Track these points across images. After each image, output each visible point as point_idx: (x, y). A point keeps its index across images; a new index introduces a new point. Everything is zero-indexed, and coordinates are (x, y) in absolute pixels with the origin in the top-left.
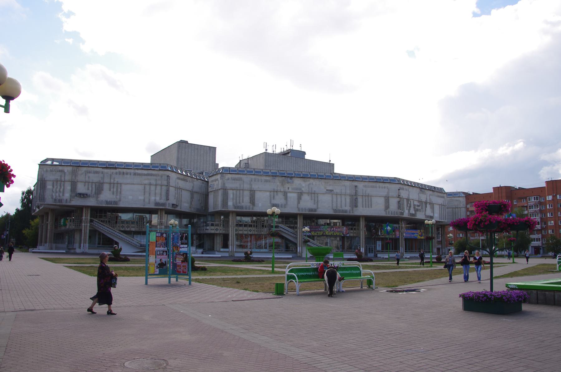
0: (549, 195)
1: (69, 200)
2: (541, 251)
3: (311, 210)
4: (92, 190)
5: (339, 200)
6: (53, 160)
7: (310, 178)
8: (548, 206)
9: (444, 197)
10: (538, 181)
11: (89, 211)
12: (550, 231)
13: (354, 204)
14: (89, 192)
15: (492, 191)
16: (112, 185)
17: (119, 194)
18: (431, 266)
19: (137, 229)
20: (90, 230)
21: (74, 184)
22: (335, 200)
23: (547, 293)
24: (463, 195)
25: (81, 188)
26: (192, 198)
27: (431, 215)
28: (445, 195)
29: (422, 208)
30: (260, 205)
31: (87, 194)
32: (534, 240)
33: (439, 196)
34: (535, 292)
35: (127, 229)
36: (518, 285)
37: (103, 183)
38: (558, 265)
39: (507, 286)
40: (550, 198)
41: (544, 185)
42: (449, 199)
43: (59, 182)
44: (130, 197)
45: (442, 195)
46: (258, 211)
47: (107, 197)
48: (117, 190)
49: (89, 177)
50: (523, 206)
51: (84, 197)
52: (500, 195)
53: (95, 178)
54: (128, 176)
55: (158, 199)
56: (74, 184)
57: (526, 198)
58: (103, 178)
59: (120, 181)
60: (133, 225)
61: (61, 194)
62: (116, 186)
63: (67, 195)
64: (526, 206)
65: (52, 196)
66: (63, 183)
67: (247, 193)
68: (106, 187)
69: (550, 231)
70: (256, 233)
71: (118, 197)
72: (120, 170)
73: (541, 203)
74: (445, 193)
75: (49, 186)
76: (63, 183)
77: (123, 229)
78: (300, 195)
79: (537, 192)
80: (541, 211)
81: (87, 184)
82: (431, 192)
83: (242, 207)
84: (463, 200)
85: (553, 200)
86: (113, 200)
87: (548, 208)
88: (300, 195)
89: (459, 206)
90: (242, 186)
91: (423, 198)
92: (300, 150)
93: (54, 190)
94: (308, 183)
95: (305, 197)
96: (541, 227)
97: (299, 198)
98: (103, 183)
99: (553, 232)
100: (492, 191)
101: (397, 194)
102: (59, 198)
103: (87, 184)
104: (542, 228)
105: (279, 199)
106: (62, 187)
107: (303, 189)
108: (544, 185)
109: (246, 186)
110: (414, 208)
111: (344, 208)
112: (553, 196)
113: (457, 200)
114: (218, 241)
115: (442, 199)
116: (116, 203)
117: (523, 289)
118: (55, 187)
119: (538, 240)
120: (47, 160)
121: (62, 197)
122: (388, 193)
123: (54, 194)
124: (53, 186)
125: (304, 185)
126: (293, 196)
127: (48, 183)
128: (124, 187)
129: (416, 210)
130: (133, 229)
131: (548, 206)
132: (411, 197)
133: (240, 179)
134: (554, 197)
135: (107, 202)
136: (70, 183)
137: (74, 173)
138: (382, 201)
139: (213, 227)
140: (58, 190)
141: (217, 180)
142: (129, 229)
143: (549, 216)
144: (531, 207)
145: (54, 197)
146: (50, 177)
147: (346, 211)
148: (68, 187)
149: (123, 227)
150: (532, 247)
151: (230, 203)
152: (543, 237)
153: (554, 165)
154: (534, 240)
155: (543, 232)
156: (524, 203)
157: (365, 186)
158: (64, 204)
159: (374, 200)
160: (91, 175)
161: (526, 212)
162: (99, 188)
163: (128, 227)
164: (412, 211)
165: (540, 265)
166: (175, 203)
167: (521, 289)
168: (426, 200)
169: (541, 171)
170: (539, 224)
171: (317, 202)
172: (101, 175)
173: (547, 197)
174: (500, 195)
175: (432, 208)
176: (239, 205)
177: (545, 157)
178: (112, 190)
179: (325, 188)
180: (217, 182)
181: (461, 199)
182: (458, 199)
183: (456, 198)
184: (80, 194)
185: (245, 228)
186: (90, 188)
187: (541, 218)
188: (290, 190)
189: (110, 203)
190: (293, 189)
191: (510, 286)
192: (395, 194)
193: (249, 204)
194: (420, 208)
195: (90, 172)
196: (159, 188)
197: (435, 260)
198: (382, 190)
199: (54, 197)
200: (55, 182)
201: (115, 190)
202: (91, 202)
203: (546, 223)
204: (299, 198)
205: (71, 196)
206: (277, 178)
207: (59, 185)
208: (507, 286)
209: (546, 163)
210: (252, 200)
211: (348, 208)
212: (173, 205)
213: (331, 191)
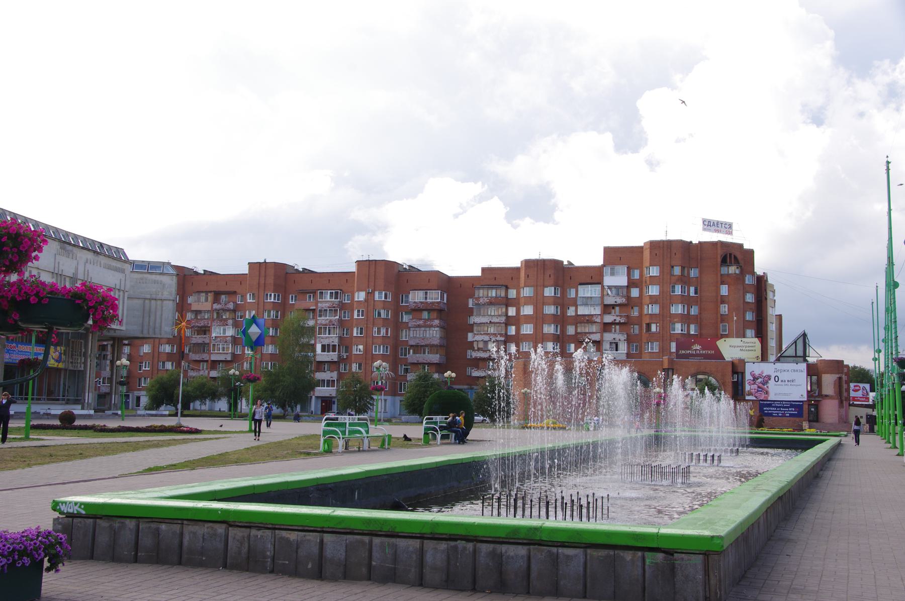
0: (359, 290)
2: (335, 407)
8: (356, 312)
9: (122, 271)
10: (345, 262)
12: (355, 367)
15: (245, 270)
18: (27, 438)
23: (163, 527)
24: (172, 271)
28: (128, 268)
32: (322, 383)
33: (109, 268)
38: (322, 439)
39: (56, 506)
40: (361, 296)
41: (353, 268)
42: (136, 276)
50: (308, 310)
52: (262, 282)
57: (314, 293)
64: (314, 310)
69: (355, 367)
73: (342, 306)
74: (127, 261)
79: (337, 282)
80: (341, 323)
82: (90, 256)
84: (171, 283)
85: (366, 300)
87: (355, 317)
89: (159, 296)
92: (664, 238)
96: (339, 356)
100: (245, 270)
104: (341, 360)
108: (353, 268)
112: (368, 294)
113: (155, 282)
115: (121, 276)
119: (330, 383)
131: (356, 312)
134: (370, 295)
143: (355, 334)
144: (323, 312)
150: (317, 397)
152: (341, 376)
154: (322, 383)
155: (342, 366)
156: (309, 303)
161: (311, 323)
165: (300, 438)
167: (95, 517)
168: (76, 273)
169: (350, 243)
170: (334, 351)
173: (356, 294)
174: (262, 282)
181: (165, 279)
182: (158, 278)
183: (153, 277)
187: (340, 338)
191: (64, 508)
197: (57, 422)
203: (348, 349)
208: (56, 506)
209: (360, 228)
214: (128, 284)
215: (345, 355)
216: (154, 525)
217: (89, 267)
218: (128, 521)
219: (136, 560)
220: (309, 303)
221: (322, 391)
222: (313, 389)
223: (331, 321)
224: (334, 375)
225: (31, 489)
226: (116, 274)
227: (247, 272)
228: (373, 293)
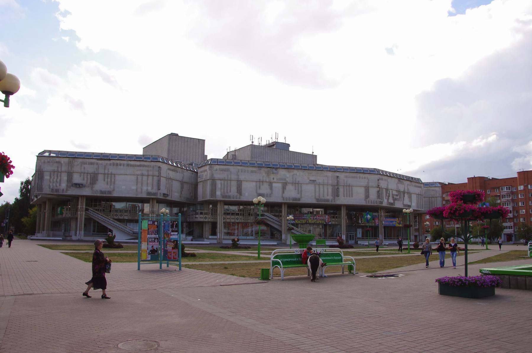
0: (520, 185)
1: (65, 190)
2: (513, 238)
3: (295, 199)
5: (321, 189)
7: (294, 169)
8: (520, 195)
9: (421, 187)
12: (521, 220)
13: (336, 193)
14: (84, 182)
15: (466, 181)
16: (106, 175)
17: (112, 184)
18: (409, 253)
19: (130, 218)
20: (85, 219)
21: (70, 175)
22: (317, 190)
23: (519, 278)
24: (439, 185)
25: (77, 179)
26: (182, 188)
27: (409, 204)
30: (247, 194)
31: (82, 185)
32: (506, 227)
33: (416, 186)
34: (507, 277)
35: (120, 218)
36: (491, 271)
38: (529, 252)
40: (521, 188)
41: (516, 176)
43: (56, 173)
44: (124, 187)
45: (417, 185)
47: (101, 187)
48: (111, 180)
49: (84, 168)
51: (80, 187)
53: (90, 169)
54: (122, 167)
55: (150, 188)
56: (70, 175)
57: (499, 188)
58: (368, 183)
59: (114, 171)
61: (58, 185)
62: (110, 177)
63: (64, 185)
64: (499, 196)
65: (49, 185)
66: (59, 174)
68: (100, 177)
69: (521, 220)
70: (243, 221)
72: (114, 161)
73: (513, 193)
75: (47, 177)
78: (285, 185)
79: (509, 182)
80: (513, 200)
82: (408, 183)
83: (229, 197)
84: (439, 190)
85: (524, 189)
87: (520, 197)
88: (285, 185)
89: (435, 196)
91: (401, 188)
93: (51, 180)
95: (290, 187)
96: (513, 215)
97: (284, 188)
99: (524, 220)
100: (466, 181)
101: (377, 184)
102: (56, 188)
103: (82, 174)
104: (514, 217)
105: (265, 189)
106: (59, 178)
107: (287, 179)
108: (516, 176)
109: (234, 177)
110: (393, 197)
111: (326, 197)
112: (525, 186)
113: (433, 190)
114: (207, 229)
116: (110, 192)
117: (496, 275)
118: (52, 177)
119: (510, 227)
120: (45, 152)
122: (368, 183)
123: (51, 184)
124: (50, 177)
125: (288, 176)
127: (45, 173)
128: (118, 178)
129: (395, 200)
130: (126, 218)
131: (520, 195)
132: (390, 187)
133: (228, 170)
134: (526, 187)
135: (101, 192)
136: (66, 174)
138: (362, 190)
139: (202, 216)
140: (55, 180)
141: (206, 170)
142: (122, 218)
144: (503, 196)
145: (52, 187)
146: (48, 168)
147: (328, 200)
148: (65, 178)
149: (116, 215)
150: (504, 234)
151: (218, 193)
152: (515, 225)
153: (525, 157)
154: (506, 227)
155: (515, 220)
156: (497, 192)
157: (346, 177)
159: (355, 189)
160: (86, 166)
161: (499, 201)
162: (94, 179)
164: (391, 201)
166: (166, 192)
167: (494, 275)
168: (404, 190)
169: (514, 162)
171: (300, 192)
172: (96, 166)
173: (519, 187)
176: (226, 194)
177: (517, 149)
178: (106, 180)
179: (308, 178)
181: (437, 189)
184: (76, 184)
186: (86, 179)
187: (513, 207)
188: (275, 180)
189: (105, 192)
190: (277, 179)
191: (483, 272)
192: (375, 184)
193: (236, 194)
194: (398, 197)
195: (85, 163)
196: (150, 178)
197: (413, 247)
198: (362, 181)
199: (52, 187)
201: (109, 180)
202: (87, 192)
203: (518, 212)
204: (284, 188)
207: (55, 175)
209: (517, 155)
210: (239, 190)
211: (330, 197)
213: (314, 181)
214: (423, 192)
215: (516, 215)
216: (515, 277)
217: (409, 187)
218: (506, 276)
219: (510, 288)
220: (497, 192)
221: (507, 231)
222: (502, 230)
223: (508, 200)
224: (512, 224)
225: (231, 284)
226: (419, 189)
227: (467, 182)
228: (527, 186)
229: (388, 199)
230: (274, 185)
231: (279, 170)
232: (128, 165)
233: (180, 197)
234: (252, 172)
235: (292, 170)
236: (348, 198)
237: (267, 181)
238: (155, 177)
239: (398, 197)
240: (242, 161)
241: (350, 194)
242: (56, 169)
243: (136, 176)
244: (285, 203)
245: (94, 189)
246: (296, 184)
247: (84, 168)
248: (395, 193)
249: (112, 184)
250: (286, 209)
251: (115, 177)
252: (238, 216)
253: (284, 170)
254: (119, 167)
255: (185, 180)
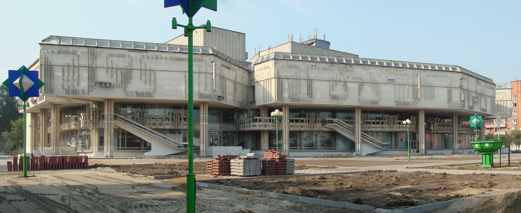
1: (86, 90)
3: (372, 102)
4: (117, 78)
5: (401, 90)
6: (60, 38)
7: (370, 65)
11: (113, 105)
13: (415, 97)
14: (113, 81)
16: (71, 68)
17: (153, 83)
19: (173, 127)
20: (114, 129)
21: (92, 70)
22: (397, 91)
25: (102, 76)
26: (235, 89)
27: (485, 108)
29: (478, 101)
30: (318, 96)
31: (110, 84)
35: (160, 127)
37: (131, 69)
43: (71, 68)
44: (167, 88)
46: (317, 103)
47: (137, 88)
48: (150, 78)
49: (112, 62)
51: (106, 87)
53: (121, 63)
54: (164, 61)
55: (202, 89)
56: (92, 70)
58: (131, 63)
59: (154, 67)
60: (167, 122)
61: (75, 84)
62: (148, 73)
63: (84, 85)
65: (63, 86)
66: (76, 69)
67: (304, 84)
68: (136, 74)
70: (308, 129)
71: (152, 87)
72: (152, 53)
75: (58, 73)
76: (76, 69)
77: (155, 127)
78: (361, 84)
81: (110, 70)
83: (299, 100)
86: (145, 91)
88: (361, 84)
90: (298, 75)
91: (479, 89)
93: (65, 78)
94: (370, 71)
95: (367, 88)
97: (360, 89)
98: (131, 69)
101: (459, 84)
102: (72, 88)
103: (110, 70)
105: (339, 91)
106: (76, 75)
107: (364, 78)
109: (303, 75)
110: (472, 100)
111: (407, 100)
114: (265, 141)
116: (149, 94)
118: (66, 74)
120: (51, 38)
121: (77, 88)
122: (131, 63)
123: (65, 83)
124: (63, 74)
125: (364, 74)
126: (353, 87)
127: (55, 68)
128: (158, 74)
129: (474, 103)
130: (168, 127)
132: (470, 89)
133: (296, 67)
135: (138, 94)
136: (87, 69)
137: (93, 56)
138: (444, 92)
139: (261, 123)
140: (70, 78)
141: (268, 67)
142: (162, 127)
145: (66, 87)
146: (57, 60)
147: (408, 104)
148: (85, 74)
149: (154, 124)
151: (286, 95)
157: (427, 76)
158: (81, 96)
159: (437, 91)
160: (114, 59)
162: (126, 75)
163: (161, 124)
164: (471, 104)
166: (220, 95)
168: (481, 92)
171: (378, 93)
172: (128, 60)
175: (486, 101)
176: (295, 96)
178: (143, 78)
179: (387, 77)
180: (268, 70)
184: (101, 83)
185: (297, 124)
186: (115, 76)
188: (350, 79)
189: (142, 94)
190: (353, 78)
192: (457, 85)
193: (306, 96)
194: (476, 100)
195: (112, 55)
196: (203, 76)
198: (444, 80)
199: (66, 87)
200: (66, 68)
201: (147, 78)
202: (118, 94)
204: (360, 89)
205: (89, 85)
206: (335, 65)
207: (71, 71)
210: (310, 92)
211: (410, 100)
212: (219, 97)
213: (393, 80)
229: (469, 104)
230: (349, 85)
231: (353, 67)
232: (171, 59)
233: (234, 101)
234: (324, 69)
235: (369, 67)
236: (427, 100)
237: (342, 80)
238: (207, 75)
239: (476, 100)
240: (284, 54)
241: (432, 97)
242: (71, 63)
243: (61, 68)
244: (358, 108)
245: (127, 89)
246: (374, 83)
247: (112, 62)
248: (474, 95)
249: (153, 83)
250: (360, 114)
251: (155, 74)
252: (302, 124)
253: (359, 67)
254: (160, 60)
255: (239, 80)
